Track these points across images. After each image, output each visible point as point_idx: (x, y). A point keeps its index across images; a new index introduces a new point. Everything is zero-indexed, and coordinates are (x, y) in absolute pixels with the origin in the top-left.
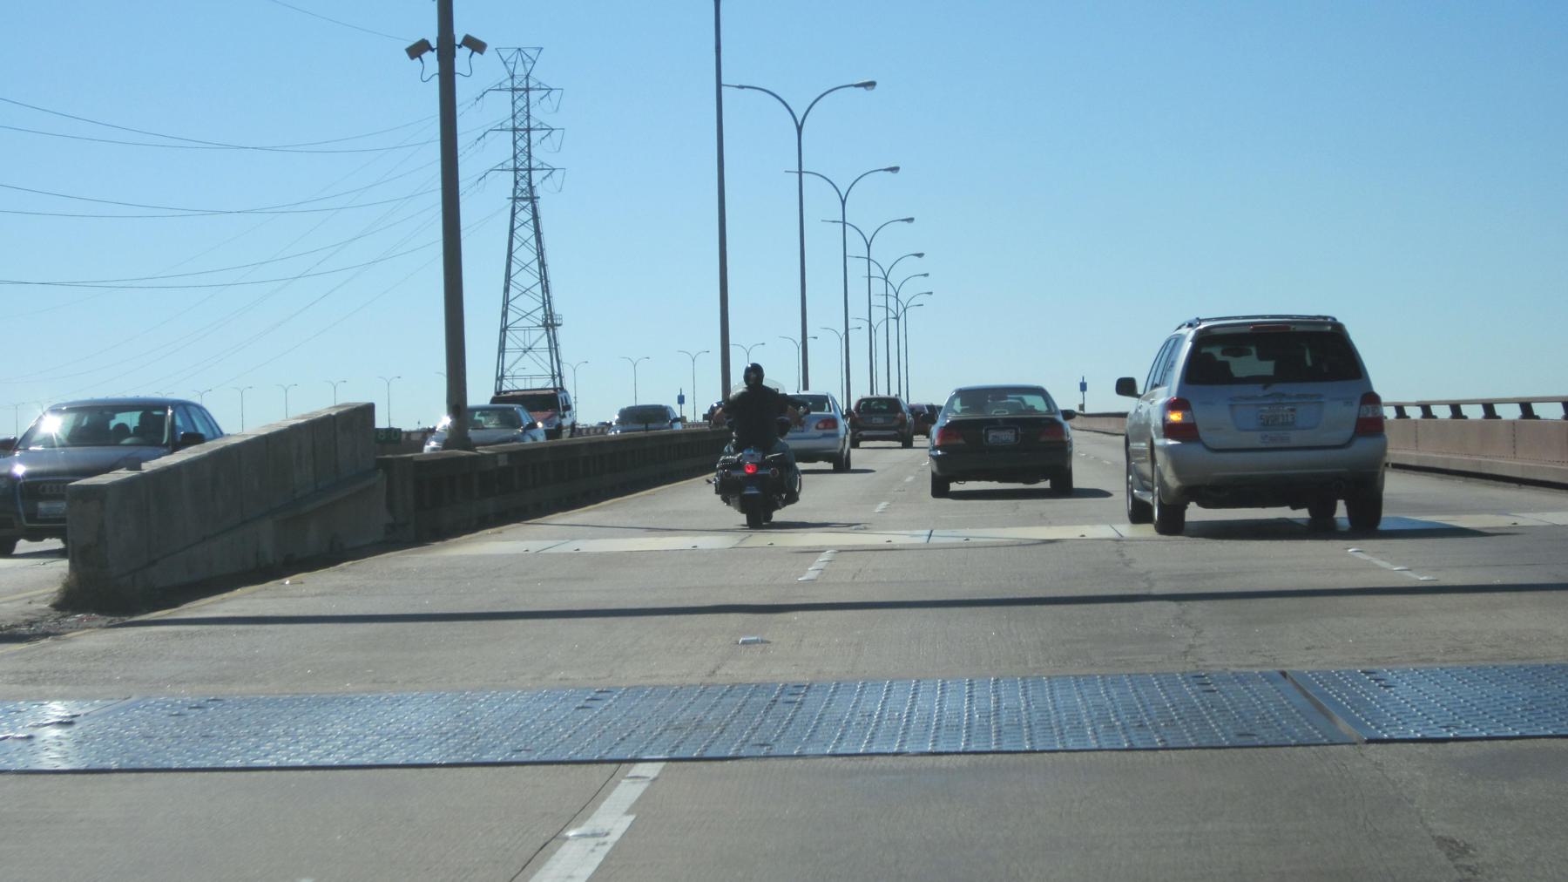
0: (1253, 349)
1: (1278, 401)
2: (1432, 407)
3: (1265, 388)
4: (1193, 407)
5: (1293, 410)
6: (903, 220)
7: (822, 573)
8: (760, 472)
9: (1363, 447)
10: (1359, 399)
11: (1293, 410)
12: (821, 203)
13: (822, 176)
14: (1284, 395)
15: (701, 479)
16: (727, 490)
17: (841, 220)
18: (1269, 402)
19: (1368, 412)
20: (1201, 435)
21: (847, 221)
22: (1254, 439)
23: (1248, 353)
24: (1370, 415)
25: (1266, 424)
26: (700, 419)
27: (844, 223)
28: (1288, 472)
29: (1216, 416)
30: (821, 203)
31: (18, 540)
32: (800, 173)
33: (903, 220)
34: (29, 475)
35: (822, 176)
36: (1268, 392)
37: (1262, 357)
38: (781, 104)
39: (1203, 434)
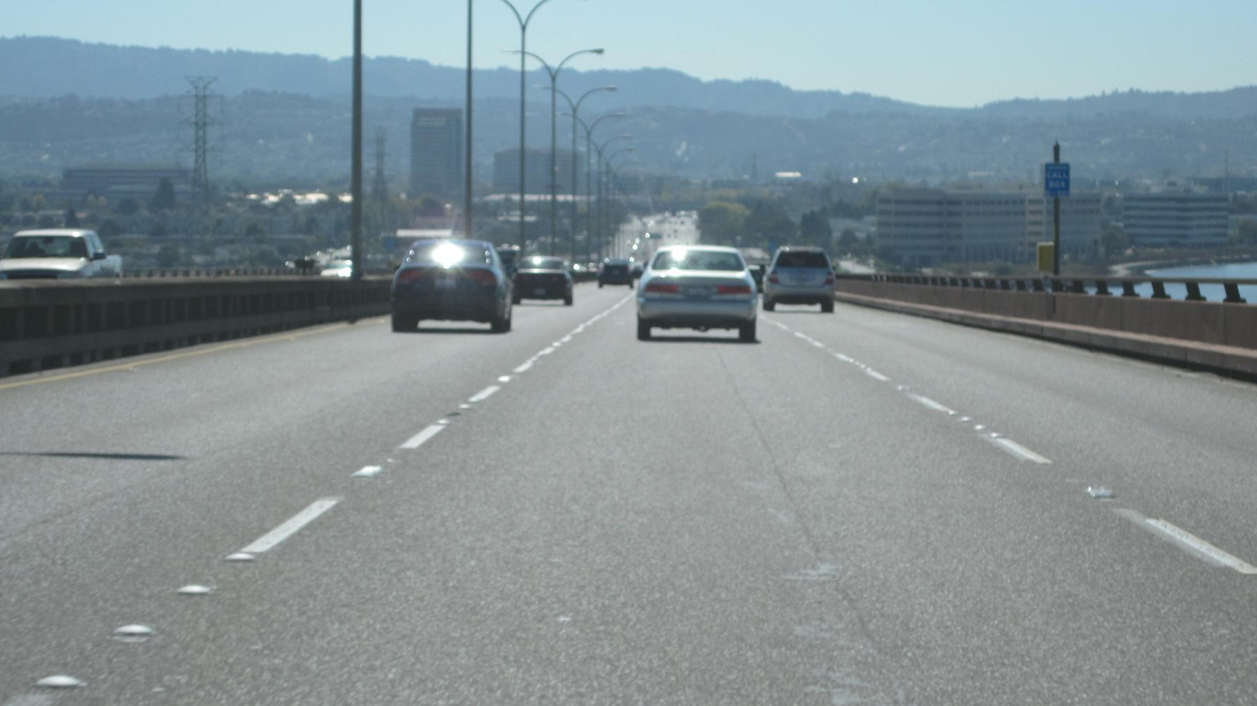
21: (527, 49)
27: (523, 53)
32: (523, 53)
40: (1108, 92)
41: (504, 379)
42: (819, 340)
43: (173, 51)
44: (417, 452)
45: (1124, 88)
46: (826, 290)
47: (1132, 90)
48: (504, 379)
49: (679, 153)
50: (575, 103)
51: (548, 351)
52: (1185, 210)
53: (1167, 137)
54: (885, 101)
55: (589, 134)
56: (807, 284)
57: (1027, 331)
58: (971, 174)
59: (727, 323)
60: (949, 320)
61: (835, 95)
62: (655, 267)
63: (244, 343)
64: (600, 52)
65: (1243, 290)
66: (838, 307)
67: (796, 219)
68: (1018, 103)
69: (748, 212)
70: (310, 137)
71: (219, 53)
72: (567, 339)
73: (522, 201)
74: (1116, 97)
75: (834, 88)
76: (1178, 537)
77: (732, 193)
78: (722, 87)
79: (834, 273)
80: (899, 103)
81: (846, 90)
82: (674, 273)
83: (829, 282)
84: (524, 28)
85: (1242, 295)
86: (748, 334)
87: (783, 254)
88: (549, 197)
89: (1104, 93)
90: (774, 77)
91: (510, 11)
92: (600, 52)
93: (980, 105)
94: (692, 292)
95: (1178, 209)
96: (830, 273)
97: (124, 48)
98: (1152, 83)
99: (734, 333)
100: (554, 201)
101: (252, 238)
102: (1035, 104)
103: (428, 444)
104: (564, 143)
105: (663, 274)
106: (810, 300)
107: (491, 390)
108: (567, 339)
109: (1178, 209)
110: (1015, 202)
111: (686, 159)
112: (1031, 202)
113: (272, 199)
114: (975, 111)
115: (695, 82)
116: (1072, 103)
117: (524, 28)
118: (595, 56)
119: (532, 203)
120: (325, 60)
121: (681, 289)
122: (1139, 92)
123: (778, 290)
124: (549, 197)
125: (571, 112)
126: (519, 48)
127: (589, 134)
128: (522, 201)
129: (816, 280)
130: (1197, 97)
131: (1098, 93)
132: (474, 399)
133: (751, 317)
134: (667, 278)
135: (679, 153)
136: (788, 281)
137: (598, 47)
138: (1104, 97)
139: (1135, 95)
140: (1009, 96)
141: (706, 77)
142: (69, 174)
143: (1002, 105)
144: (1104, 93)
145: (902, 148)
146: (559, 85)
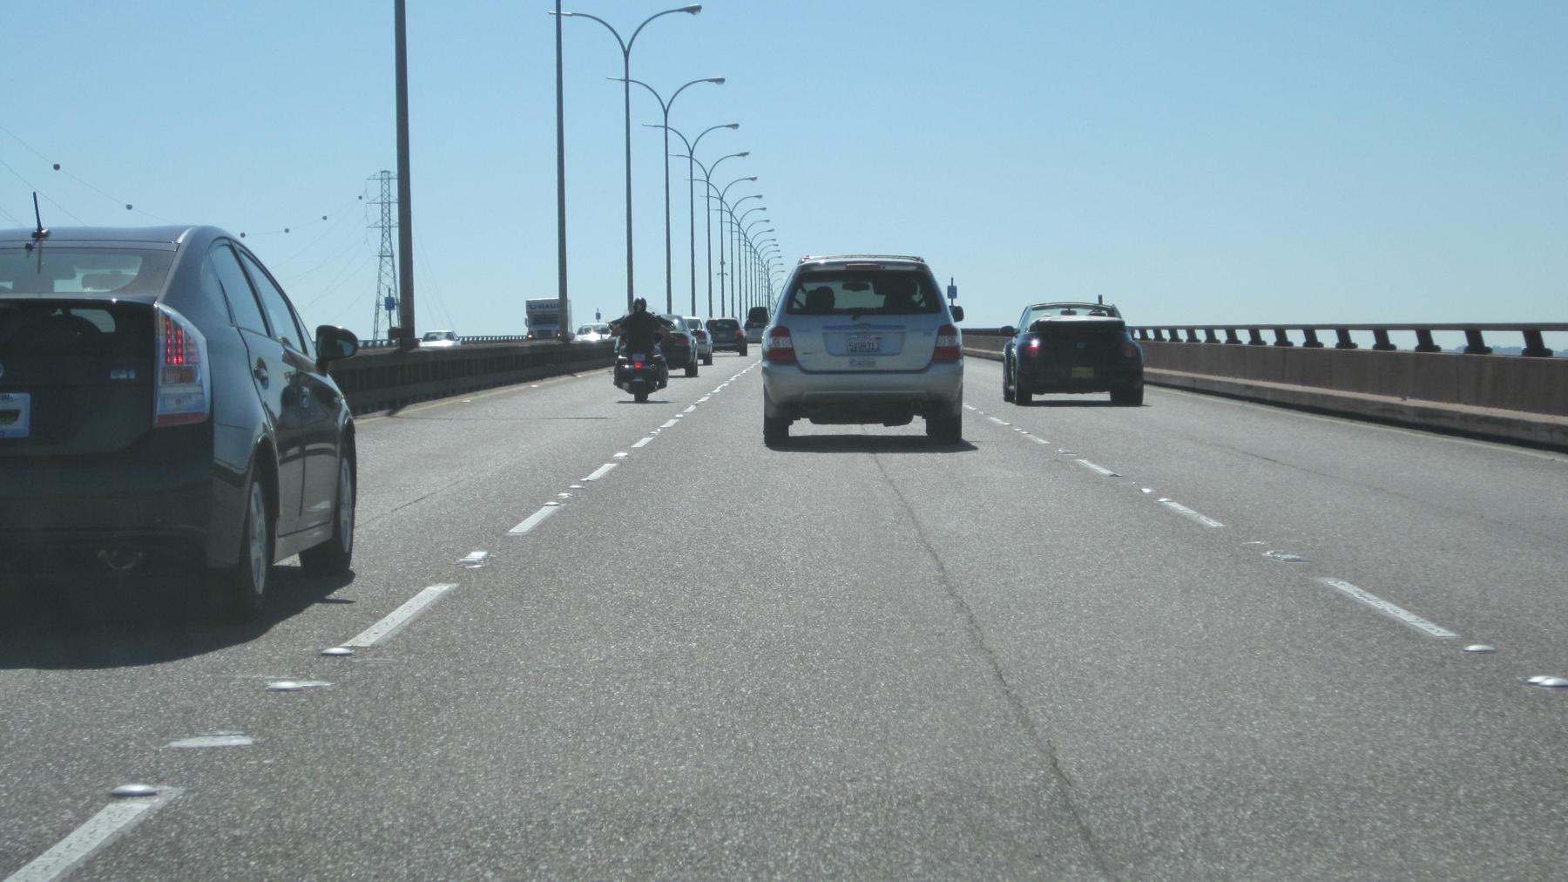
0: (871, 285)
1: (865, 330)
2: (1237, 331)
3: (854, 319)
4: (792, 334)
5: (878, 339)
6: (728, 126)
7: (619, 467)
8: (644, 367)
9: (940, 373)
10: (938, 328)
11: (878, 339)
12: (646, 110)
13: (645, 85)
14: (870, 326)
15: (605, 371)
16: (621, 380)
17: (664, 125)
18: (858, 331)
19: (945, 342)
20: (798, 359)
21: (669, 126)
22: (843, 363)
23: (867, 288)
24: (947, 344)
25: (854, 351)
26: (384, 335)
27: (666, 127)
28: (900, 392)
29: (811, 343)
30: (646, 110)
31: (804, 417)
32: (627, 80)
33: (728, 126)
34: (117, 302)
35: (645, 85)
36: (857, 322)
37: (878, 291)
38: (598, 23)
39: (799, 355)
41: (621, 455)
42: (1210, 514)
44: (525, 537)
48: (621, 455)
51: (671, 423)
57: (1198, 386)
60: (1259, 399)
63: (592, 373)
65: (1550, 340)
66: (1149, 394)
72: (692, 408)
79: (959, 325)
84: (626, 54)
85: (1354, 340)
92: (760, 197)
103: (540, 528)
107: (607, 467)
108: (692, 408)
117: (666, 113)
125: (706, 179)
126: (624, 77)
127: (691, 153)
137: (763, 207)
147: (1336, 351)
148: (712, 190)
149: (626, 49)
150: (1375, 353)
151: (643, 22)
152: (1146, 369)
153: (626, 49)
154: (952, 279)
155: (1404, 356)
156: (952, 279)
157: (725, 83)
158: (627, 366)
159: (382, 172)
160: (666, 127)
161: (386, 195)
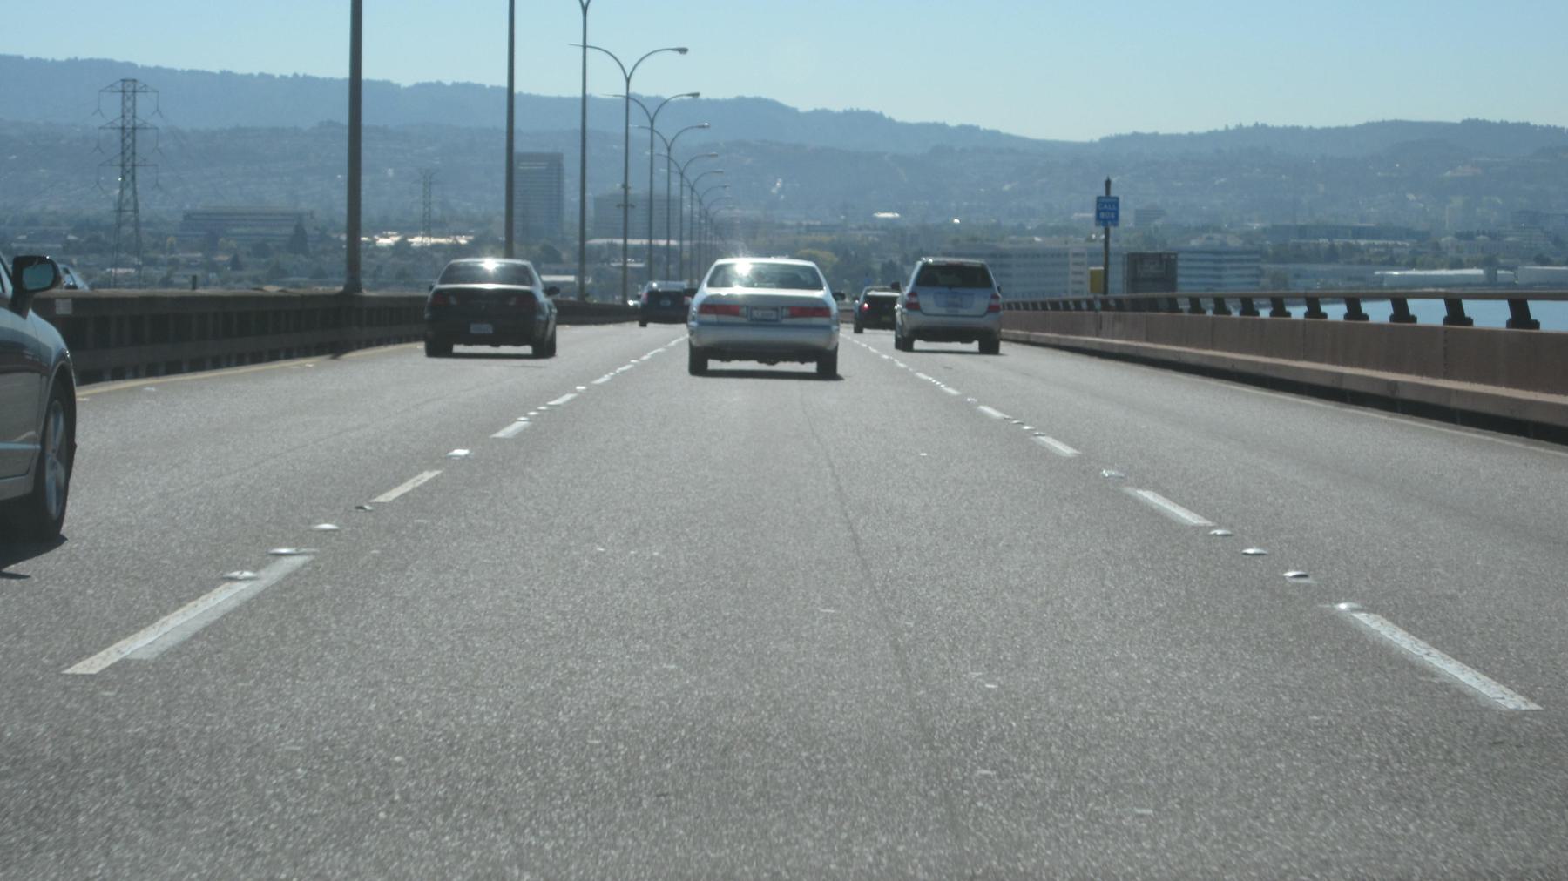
27: (652, 130)
32: (585, 47)
40: (1232, 126)
43: (236, 75)
45: (1248, 122)
46: (988, 321)
47: (1256, 124)
49: (774, 191)
50: (669, 138)
52: (1220, 261)
53: (1284, 176)
54: (995, 134)
55: (652, 122)
56: (962, 311)
58: (1076, 215)
59: (802, 354)
61: (941, 128)
62: (711, 284)
64: (683, 51)
66: (1004, 347)
67: (877, 267)
68: (1136, 137)
69: (836, 260)
70: (390, 172)
71: (284, 78)
73: (625, 246)
74: (1241, 131)
75: (940, 120)
76: (1462, 678)
77: (825, 238)
78: (822, 116)
80: (1010, 137)
81: (953, 122)
82: (737, 290)
83: (993, 309)
84: (628, 80)
85: (1412, 311)
86: (828, 369)
87: (926, 267)
88: (645, 242)
89: (1227, 127)
90: (876, 108)
91: (616, 63)
92: (683, 51)
93: (1096, 139)
94: (758, 314)
95: (1215, 261)
96: (995, 297)
97: (183, 72)
98: (1278, 118)
99: (811, 367)
100: (650, 246)
101: (402, 282)
102: (1154, 138)
104: (660, 187)
105: (724, 292)
106: (963, 335)
109: (1215, 261)
110: (1059, 255)
111: (782, 197)
112: (1076, 255)
113: (886, 357)
114: (1091, 145)
115: (793, 112)
116: (1192, 138)
117: (628, 80)
118: (677, 53)
119: (636, 248)
120: (398, 86)
121: (744, 310)
122: (1264, 127)
123: (917, 319)
124: (645, 242)
126: (588, 50)
127: (652, 122)
128: (625, 246)
129: (975, 305)
130: (1326, 133)
131: (1221, 128)
132: (381, 499)
133: (831, 348)
134: (729, 296)
135: (774, 191)
136: (934, 307)
137: (694, 91)
138: (1227, 131)
139: (1260, 130)
140: (1125, 129)
141: (804, 106)
142: (188, 216)
143: (1118, 140)
144: (1227, 127)
145: (1007, 187)
146: (657, 126)
147: (1505, 333)
148: (694, 194)
149: (628, 75)
150: (1391, 326)
151: (647, 53)
152: (1003, 330)
153: (628, 75)
154: (1108, 183)
155: (1489, 335)
156: (1108, 183)
157: (688, 53)
158: (1037, 239)
159: (124, 81)
160: (652, 130)
161: (129, 117)
